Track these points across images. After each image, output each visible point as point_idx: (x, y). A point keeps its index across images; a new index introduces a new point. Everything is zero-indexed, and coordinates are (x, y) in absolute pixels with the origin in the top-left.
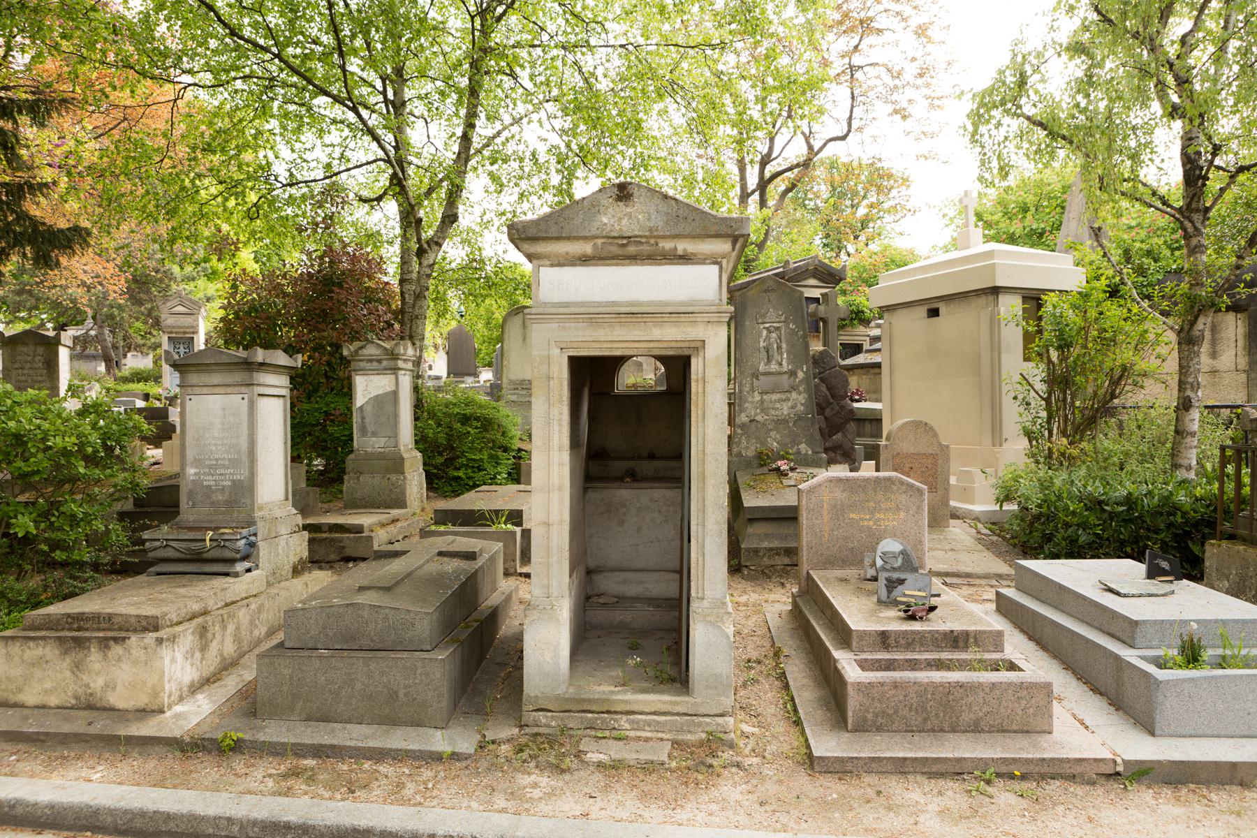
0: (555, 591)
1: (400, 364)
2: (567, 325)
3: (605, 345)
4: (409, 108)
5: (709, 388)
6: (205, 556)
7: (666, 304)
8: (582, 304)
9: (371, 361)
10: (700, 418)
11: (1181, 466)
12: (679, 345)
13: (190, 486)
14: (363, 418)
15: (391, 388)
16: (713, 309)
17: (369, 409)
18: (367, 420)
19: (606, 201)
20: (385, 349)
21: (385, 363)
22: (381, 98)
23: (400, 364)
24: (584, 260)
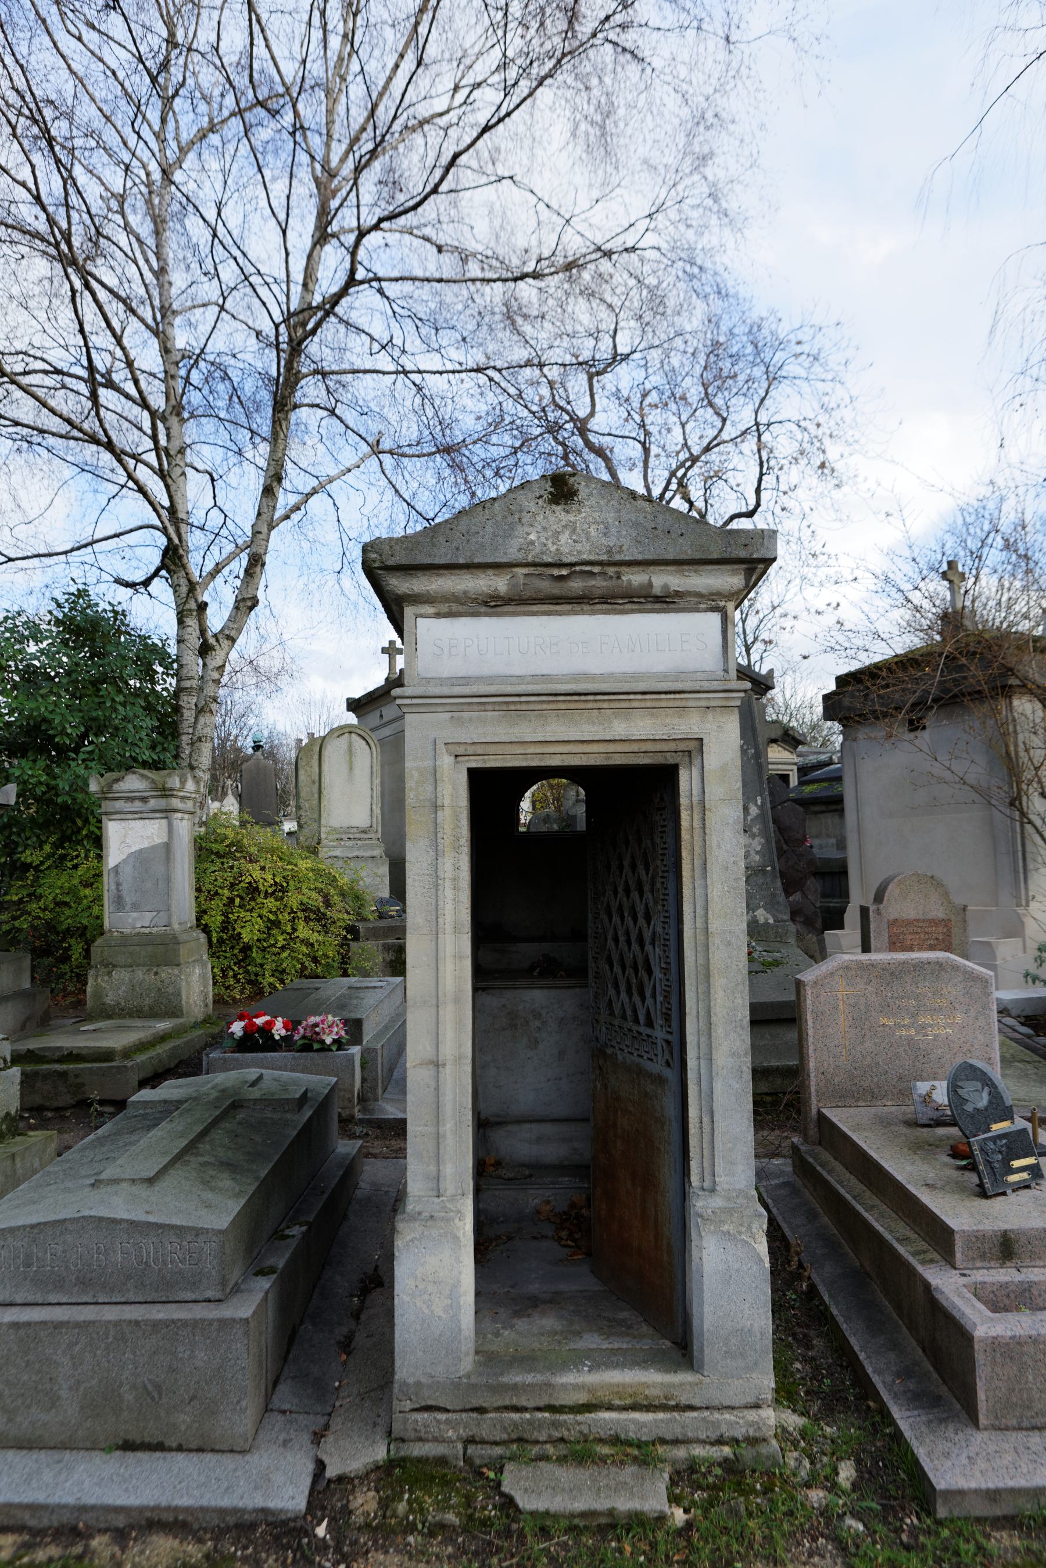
0: (449, 1187)
3: (531, 749)
4: (190, 456)
5: (712, 819)
7: (635, 677)
8: (491, 679)
9: (131, 799)
10: (698, 872)
12: (659, 747)
14: (118, 884)
16: (715, 685)
17: (127, 872)
18: (125, 887)
19: (527, 502)
20: (153, 782)
21: (153, 803)
22: (149, 444)
24: (493, 605)
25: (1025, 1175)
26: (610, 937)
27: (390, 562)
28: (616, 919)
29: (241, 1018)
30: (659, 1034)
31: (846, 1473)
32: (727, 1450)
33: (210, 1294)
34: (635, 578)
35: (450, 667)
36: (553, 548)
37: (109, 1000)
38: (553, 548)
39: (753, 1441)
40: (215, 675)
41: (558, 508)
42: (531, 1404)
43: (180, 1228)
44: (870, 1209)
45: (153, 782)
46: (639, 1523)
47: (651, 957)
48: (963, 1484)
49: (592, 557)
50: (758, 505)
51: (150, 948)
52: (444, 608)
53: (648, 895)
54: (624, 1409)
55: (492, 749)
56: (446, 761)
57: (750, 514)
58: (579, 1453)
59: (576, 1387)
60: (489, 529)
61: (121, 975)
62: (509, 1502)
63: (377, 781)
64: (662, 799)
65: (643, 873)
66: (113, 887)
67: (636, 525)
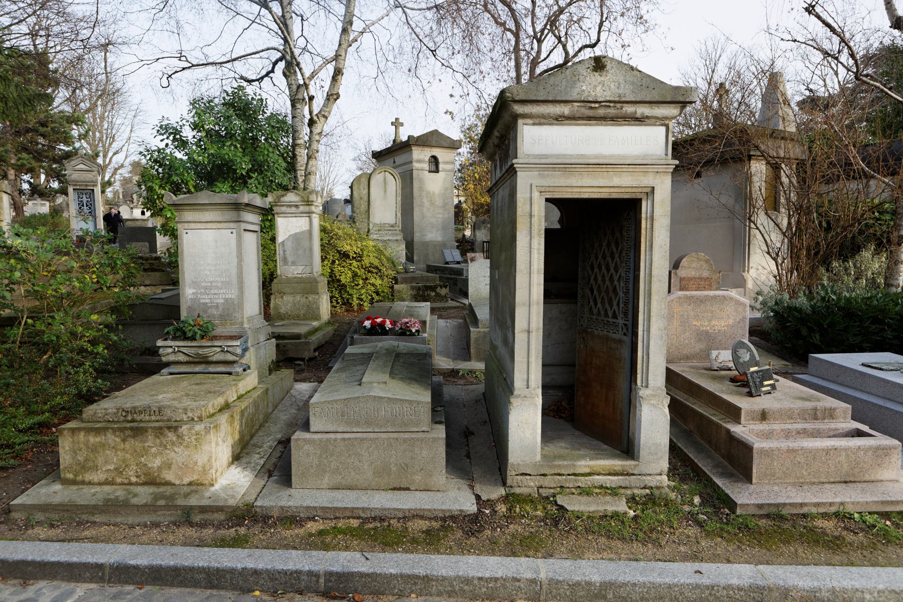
1: (313, 208)
2: (546, 173)
5: (656, 225)
6: (211, 359)
7: (625, 157)
9: (291, 206)
11: (892, 285)
12: (634, 190)
13: (189, 304)
14: (284, 251)
15: (306, 227)
16: (662, 162)
17: (289, 245)
18: (288, 253)
21: (301, 208)
23: (313, 208)
24: (559, 119)
25: (769, 388)
26: (592, 278)
27: (517, 98)
28: (596, 270)
29: (368, 319)
30: (620, 321)
31: (697, 500)
32: (648, 491)
33: (424, 429)
34: (629, 109)
35: (538, 150)
36: (593, 94)
37: (282, 311)
38: (593, 94)
39: (658, 488)
40: (317, 138)
41: (597, 74)
42: (566, 473)
43: (410, 401)
44: (694, 404)
45: (302, 197)
46: (615, 515)
47: (618, 287)
48: (748, 502)
49: (611, 99)
50: (598, 40)
51: (303, 285)
52: (537, 121)
53: (617, 259)
54: (605, 475)
55: (557, 189)
56: (536, 194)
57: (593, 46)
58: (585, 492)
59: (585, 466)
60: (564, 83)
61: (288, 298)
62: (561, 508)
63: (399, 199)
64: (628, 214)
65: (614, 249)
66: (281, 252)
67: (633, 83)
